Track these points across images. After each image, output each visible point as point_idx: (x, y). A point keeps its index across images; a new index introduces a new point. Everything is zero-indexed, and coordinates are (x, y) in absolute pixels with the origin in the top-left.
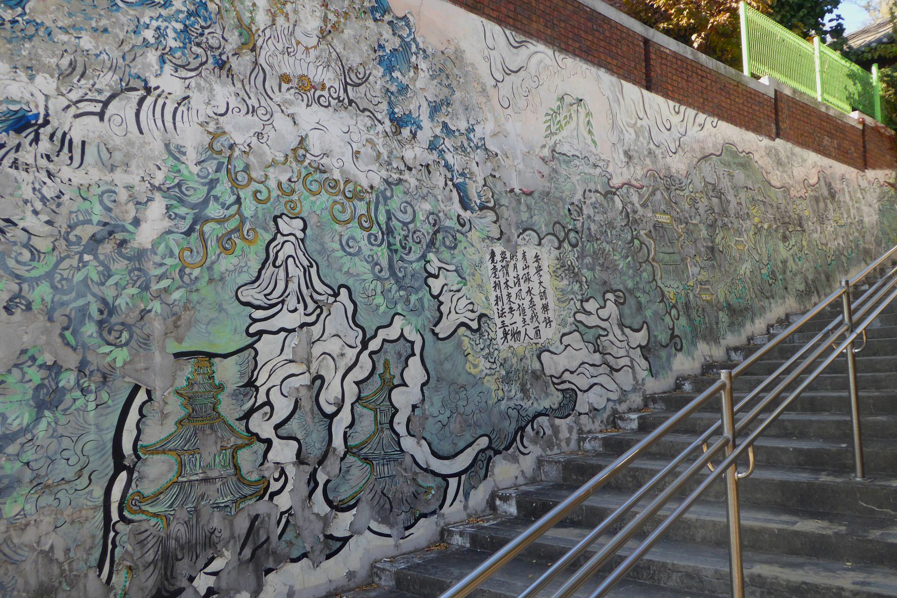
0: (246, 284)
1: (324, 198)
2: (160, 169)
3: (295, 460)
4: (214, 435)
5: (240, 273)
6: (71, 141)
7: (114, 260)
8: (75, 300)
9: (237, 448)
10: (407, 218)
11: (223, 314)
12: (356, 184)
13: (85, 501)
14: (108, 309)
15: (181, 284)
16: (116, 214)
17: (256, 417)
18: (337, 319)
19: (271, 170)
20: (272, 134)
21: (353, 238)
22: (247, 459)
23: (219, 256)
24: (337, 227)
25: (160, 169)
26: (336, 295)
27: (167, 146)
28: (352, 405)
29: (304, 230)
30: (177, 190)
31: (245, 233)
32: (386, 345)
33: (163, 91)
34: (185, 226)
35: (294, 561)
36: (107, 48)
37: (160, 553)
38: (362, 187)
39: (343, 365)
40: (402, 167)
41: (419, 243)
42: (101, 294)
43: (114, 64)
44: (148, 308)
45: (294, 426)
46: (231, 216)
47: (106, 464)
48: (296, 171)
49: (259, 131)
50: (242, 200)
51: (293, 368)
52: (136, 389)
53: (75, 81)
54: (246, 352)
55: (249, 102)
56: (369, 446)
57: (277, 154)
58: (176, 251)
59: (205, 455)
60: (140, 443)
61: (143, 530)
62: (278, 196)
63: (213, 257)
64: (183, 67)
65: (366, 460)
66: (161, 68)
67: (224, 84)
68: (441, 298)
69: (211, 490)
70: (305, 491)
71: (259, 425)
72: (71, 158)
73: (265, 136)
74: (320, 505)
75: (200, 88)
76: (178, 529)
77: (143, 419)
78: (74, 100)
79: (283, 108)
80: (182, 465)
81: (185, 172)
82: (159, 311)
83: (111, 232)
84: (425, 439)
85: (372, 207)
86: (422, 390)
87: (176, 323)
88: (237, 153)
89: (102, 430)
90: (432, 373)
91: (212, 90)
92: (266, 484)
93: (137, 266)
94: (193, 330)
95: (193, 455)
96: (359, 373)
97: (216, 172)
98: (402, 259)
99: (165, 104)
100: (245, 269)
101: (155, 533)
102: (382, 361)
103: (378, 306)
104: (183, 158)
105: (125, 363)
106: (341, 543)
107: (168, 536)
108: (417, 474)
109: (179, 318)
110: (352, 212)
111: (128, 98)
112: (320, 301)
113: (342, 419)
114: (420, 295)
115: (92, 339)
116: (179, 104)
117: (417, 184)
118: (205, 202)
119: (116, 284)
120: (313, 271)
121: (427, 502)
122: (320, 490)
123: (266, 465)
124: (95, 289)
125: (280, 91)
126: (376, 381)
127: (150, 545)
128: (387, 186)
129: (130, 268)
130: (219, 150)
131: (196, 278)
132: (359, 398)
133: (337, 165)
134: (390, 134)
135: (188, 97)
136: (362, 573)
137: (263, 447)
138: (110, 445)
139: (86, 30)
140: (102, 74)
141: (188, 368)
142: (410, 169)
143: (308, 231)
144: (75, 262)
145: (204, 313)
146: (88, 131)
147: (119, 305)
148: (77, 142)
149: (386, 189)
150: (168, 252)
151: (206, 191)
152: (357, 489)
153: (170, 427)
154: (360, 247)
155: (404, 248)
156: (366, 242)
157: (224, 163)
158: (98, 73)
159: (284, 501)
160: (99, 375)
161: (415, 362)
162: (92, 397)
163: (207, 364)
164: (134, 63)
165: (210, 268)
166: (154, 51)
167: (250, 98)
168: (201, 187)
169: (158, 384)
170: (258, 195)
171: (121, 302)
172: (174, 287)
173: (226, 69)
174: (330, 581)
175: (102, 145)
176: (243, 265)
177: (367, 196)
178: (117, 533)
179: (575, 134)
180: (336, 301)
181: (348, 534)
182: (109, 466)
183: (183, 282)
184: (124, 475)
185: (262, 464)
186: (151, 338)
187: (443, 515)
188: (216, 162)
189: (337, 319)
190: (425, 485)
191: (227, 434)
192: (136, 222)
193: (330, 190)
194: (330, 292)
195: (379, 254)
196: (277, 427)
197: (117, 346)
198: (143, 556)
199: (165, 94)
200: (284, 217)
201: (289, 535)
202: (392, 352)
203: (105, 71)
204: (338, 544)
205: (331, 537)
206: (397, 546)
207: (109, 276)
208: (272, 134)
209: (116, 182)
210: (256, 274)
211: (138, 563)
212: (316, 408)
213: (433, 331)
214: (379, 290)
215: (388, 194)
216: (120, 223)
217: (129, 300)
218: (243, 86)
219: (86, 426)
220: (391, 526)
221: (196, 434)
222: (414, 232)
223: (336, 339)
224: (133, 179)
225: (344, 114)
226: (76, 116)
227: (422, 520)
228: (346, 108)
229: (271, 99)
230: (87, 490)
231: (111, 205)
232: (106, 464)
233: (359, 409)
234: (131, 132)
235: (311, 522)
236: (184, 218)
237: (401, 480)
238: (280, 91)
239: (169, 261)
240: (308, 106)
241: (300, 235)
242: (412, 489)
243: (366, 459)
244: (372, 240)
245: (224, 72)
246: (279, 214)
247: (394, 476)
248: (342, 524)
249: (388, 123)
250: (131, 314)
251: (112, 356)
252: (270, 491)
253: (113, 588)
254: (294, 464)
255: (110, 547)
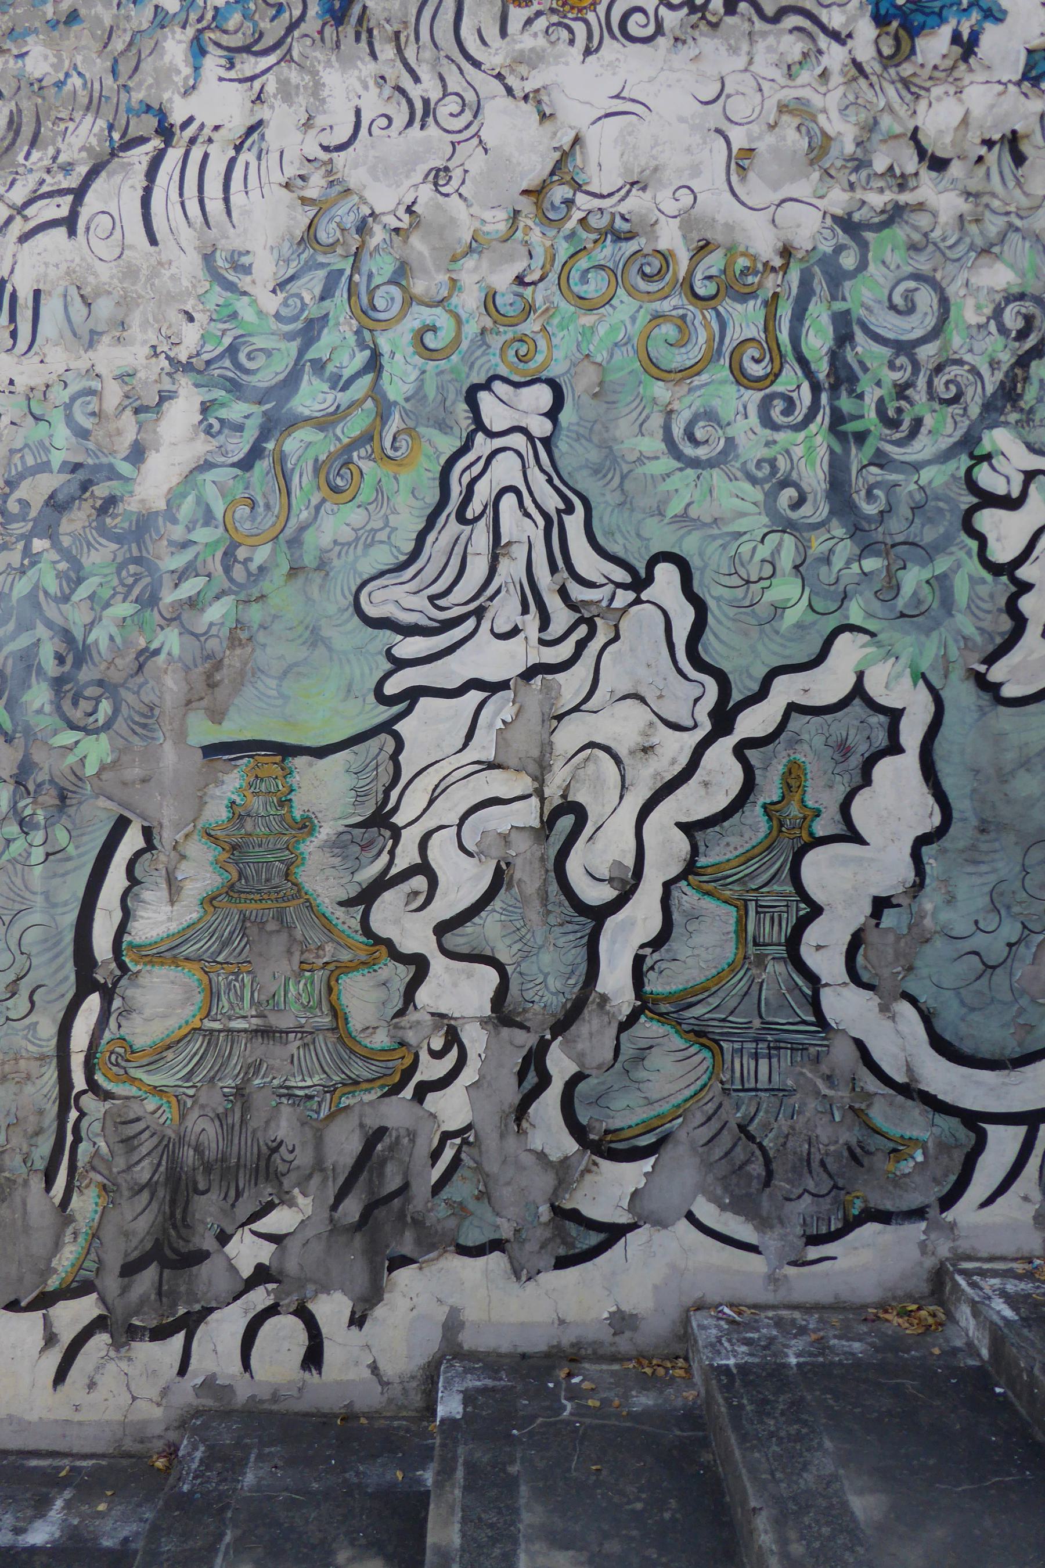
0: (382, 574)
1: (625, 312)
2: (191, 319)
3: (488, 1012)
4: (284, 936)
5: (368, 546)
6: (14, 296)
7: (89, 544)
8: (13, 637)
9: (338, 970)
10: (912, 327)
11: (321, 650)
12: (731, 251)
13: (24, 1043)
14: (75, 651)
15: (227, 585)
16: (97, 444)
17: (390, 900)
18: (639, 649)
19: (470, 262)
20: (477, 162)
21: (710, 416)
22: (364, 998)
23: (318, 508)
24: (660, 391)
25: (191, 319)
26: (640, 583)
27: (208, 259)
28: (667, 886)
29: (553, 414)
30: (227, 363)
31: (387, 444)
32: (797, 722)
33: (202, 126)
34: (240, 446)
35: (464, 1251)
36: (79, 59)
37: (162, 1169)
38: (754, 258)
39: (645, 779)
40: (910, 163)
41: (955, 400)
42: (59, 620)
43: (96, 95)
44: (154, 646)
45: (490, 930)
46: (354, 405)
47: (60, 976)
48: (539, 252)
49: (440, 163)
50: (385, 360)
51: (497, 784)
52: (121, 825)
53: (20, 158)
54: (373, 744)
55: (416, 93)
56: (714, 1001)
57: (488, 215)
58: (219, 508)
59: (265, 977)
60: (127, 938)
61: (132, 1116)
62: (483, 331)
63: (304, 515)
64: (247, 49)
65: (700, 1035)
66: (197, 69)
67: (347, 63)
68: (1024, 573)
69: (277, 1054)
70: (511, 1094)
71: (397, 922)
72: (14, 335)
73: (457, 174)
74: (548, 1130)
75: (287, 93)
76: (203, 1129)
77: (136, 889)
78: (19, 202)
79: (510, 80)
80: (212, 994)
81: (248, 314)
82: (176, 652)
83: (87, 483)
84: (913, 1001)
85: (785, 311)
86: (916, 855)
87: (212, 680)
88: (378, 236)
89: (54, 905)
90: (960, 805)
91: (318, 85)
92: (408, 1061)
93: (135, 553)
94: (248, 691)
95: (237, 974)
96: (694, 802)
97: (322, 299)
98: (881, 460)
99: (206, 156)
100: (382, 536)
101: (154, 1126)
102: (778, 768)
103: (778, 610)
104: (244, 282)
105: (103, 768)
106: (602, 1236)
107: (181, 1139)
108: (869, 1096)
109: (218, 665)
110: (710, 340)
111: (127, 167)
112: (586, 603)
113: (632, 923)
114: (942, 565)
115: (41, 717)
116: (238, 148)
117: (965, 206)
118: (291, 381)
119: (92, 597)
120: (574, 523)
121: (897, 1181)
122: (553, 1094)
123: (412, 1016)
124: (51, 611)
125: (504, 33)
126: (753, 825)
127: (144, 1150)
128: (843, 238)
129: (119, 559)
130: (336, 246)
131: (261, 569)
132: (690, 869)
133: (670, 207)
134: (873, 67)
135: (260, 123)
136: (657, 1326)
137: (404, 973)
138: (69, 937)
139: (36, 31)
140: (71, 126)
141: (232, 782)
142: (939, 164)
143: (565, 416)
144: (15, 557)
145: (275, 651)
146: (46, 264)
147: (96, 642)
148: (25, 297)
149: (839, 249)
150: (200, 514)
151: (294, 353)
152: (665, 1107)
153: (188, 911)
154: (730, 441)
155: (893, 424)
156: (754, 419)
157: (341, 272)
158: (62, 126)
159: (452, 1108)
160: (54, 792)
161: (898, 778)
162: (38, 837)
163: (276, 770)
164: (137, 78)
165: (295, 542)
166: (178, 30)
167: (417, 79)
168: (283, 345)
169: (168, 815)
170: (430, 340)
171: (99, 636)
172: (211, 595)
173: (354, 20)
174: (562, 1322)
175: (73, 291)
176: (378, 524)
177: (771, 283)
178: (82, 1114)
179: (168, 954)
180: (638, 601)
181: (623, 1218)
182: (66, 978)
183: (231, 580)
184: (93, 1002)
185: (401, 1013)
186: (157, 712)
187: (953, 1226)
188: (322, 273)
189: (639, 649)
190: (894, 1131)
191: (315, 936)
192: (138, 454)
193: (642, 285)
194: (621, 575)
195: (798, 452)
196: (442, 929)
197: (87, 731)
198: (129, 1168)
199: (207, 132)
200: (498, 386)
201: (460, 1189)
202: (818, 741)
203: (77, 116)
204: (594, 1239)
205: (575, 1216)
206: (773, 1280)
207: (79, 581)
208: (477, 162)
209: (98, 369)
210: (410, 546)
211: (120, 1180)
212: (554, 887)
213: (981, 681)
214: (787, 558)
215: (848, 261)
216: (104, 460)
217: (114, 631)
218: (400, 51)
219: (27, 895)
220: (763, 1224)
221: (243, 928)
222: (939, 369)
223: (632, 705)
224: (133, 355)
225: (708, 44)
226: (24, 238)
227: (871, 1229)
228: (714, 26)
229: (477, 64)
230: (27, 1021)
231: (87, 423)
232: (60, 976)
233: (687, 897)
234: (132, 247)
235: (520, 1168)
236: (239, 428)
237: (812, 1104)
238: (504, 33)
239: (202, 535)
240: (588, 52)
241: (541, 427)
242: (849, 1136)
243: (700, 1034)
244: (776, 414)
245: (349, 30)
246: (482, 379)
247: (789, 1092)
248: (609, 1190)
249: (866, 30)
250: (117, 661)
251: (79, 751)
252: (417, 1078)
253: (69, 1220)
254: (484, 1022)
255: (69, 1138)
